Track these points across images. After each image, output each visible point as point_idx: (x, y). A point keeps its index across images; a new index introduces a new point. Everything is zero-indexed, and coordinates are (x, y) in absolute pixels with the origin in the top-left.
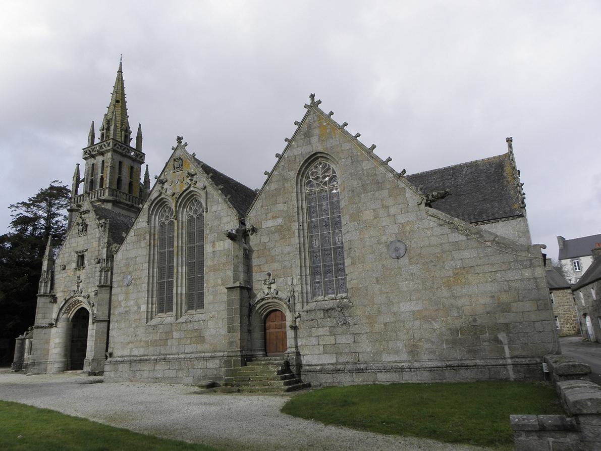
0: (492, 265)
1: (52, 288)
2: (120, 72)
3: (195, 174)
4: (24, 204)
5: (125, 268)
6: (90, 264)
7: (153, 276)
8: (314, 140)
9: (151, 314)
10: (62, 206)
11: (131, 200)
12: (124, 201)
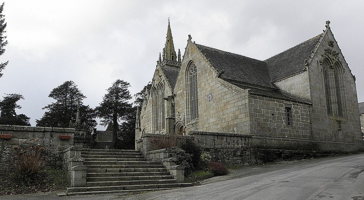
0: (234, 100)
1: (140, 126)
2: (169, 26)
3: (162, 76)
4: (139, 94)
7: (154, 117)
9: (154, 131)
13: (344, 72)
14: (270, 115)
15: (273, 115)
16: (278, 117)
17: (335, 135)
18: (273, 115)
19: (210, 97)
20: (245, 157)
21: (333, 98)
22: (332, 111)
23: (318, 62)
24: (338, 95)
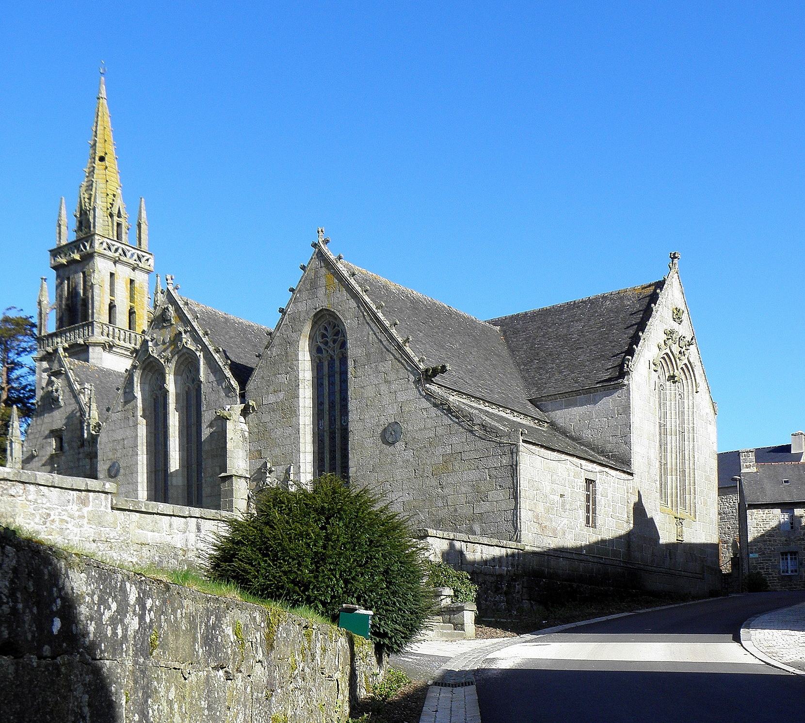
5: (111, 453)
6: (72, 448)
8: (321, 292)
10: (25, 350)
11: (133, 341)
12: (122, 343)
14: (557, 498)
15: (562, 496)
18: (562, 496)
19: (390, 435)
21: (671, 460)
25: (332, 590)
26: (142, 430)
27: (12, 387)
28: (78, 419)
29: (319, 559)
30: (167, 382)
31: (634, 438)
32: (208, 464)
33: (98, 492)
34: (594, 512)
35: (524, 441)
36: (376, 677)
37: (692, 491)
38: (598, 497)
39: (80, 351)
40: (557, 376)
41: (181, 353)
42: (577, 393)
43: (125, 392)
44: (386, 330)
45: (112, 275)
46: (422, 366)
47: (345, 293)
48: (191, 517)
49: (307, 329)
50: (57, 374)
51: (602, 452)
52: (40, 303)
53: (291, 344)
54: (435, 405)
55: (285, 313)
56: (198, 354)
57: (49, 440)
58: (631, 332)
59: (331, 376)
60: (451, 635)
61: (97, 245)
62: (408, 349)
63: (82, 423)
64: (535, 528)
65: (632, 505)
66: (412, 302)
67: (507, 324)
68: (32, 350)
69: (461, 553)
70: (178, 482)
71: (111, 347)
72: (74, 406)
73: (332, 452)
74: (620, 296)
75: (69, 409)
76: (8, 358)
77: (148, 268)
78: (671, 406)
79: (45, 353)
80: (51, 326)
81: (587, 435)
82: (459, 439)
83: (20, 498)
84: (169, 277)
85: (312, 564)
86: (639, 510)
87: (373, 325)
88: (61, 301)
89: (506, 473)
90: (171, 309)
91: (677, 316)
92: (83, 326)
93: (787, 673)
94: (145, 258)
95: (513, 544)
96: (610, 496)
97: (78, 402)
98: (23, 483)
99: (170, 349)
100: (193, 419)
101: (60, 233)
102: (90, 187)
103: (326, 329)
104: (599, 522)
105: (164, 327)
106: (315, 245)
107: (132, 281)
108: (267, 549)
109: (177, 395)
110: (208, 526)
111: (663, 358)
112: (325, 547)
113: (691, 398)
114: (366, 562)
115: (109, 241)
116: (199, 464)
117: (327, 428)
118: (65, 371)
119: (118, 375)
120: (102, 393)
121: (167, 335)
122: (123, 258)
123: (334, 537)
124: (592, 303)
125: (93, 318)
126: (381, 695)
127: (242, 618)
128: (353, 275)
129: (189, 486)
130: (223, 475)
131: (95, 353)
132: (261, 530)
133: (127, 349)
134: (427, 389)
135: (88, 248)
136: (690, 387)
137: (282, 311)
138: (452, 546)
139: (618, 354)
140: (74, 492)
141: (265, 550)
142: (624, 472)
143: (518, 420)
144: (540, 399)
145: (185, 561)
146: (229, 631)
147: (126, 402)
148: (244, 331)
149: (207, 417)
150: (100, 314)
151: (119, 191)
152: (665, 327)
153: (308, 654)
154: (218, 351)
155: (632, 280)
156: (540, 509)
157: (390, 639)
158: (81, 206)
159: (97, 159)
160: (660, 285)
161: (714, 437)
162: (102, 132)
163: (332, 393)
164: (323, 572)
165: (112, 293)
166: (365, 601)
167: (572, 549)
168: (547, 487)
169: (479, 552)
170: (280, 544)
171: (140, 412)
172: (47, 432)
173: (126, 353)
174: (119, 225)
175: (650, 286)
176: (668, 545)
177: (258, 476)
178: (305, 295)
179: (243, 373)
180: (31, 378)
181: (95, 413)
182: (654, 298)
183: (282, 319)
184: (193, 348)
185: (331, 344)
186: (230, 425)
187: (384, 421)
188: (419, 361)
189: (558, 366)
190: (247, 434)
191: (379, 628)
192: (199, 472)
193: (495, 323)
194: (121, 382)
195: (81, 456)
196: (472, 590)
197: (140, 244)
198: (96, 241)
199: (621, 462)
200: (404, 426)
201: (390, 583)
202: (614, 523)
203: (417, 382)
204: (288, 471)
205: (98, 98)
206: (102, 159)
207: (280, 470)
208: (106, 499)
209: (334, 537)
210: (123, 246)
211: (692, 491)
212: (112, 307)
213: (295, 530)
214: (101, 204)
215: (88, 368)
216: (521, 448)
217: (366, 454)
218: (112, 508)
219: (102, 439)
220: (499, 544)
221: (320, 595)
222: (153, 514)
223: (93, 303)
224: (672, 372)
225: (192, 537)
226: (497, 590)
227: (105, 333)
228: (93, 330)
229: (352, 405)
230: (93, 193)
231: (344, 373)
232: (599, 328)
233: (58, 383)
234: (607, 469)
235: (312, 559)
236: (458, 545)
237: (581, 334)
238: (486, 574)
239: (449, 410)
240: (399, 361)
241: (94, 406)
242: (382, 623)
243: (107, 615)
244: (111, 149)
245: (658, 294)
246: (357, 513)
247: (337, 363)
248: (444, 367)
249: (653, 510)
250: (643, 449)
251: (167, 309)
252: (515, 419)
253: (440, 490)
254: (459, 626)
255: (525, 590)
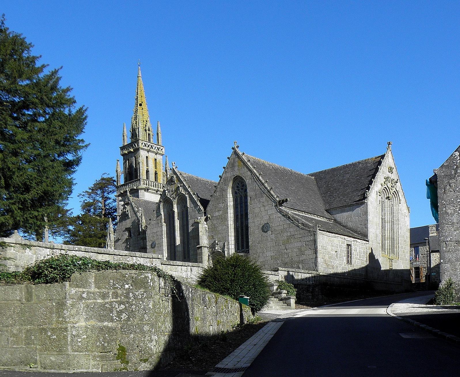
6: (134, 235)
8: (236, 168)
10: (111, 191)
11: (157, 187)
13: (400, 203)
14: (334, 252)
15: (336, 252)
16: (340, 255)
17: (386, 275)
18: (336, 252)
19: (265, 228)
20: (315, 294)
21: (387, 234)
22: (385, 248)
23: (378, 192)
24: (392, 229)
25: (236, 291)
26: (164, 228)
27: (106, 208)
28: (137, 224)
29: (232, 281)
30: (174, 208)
31: (369, 225)
32: (192, 242)
33: (156, 258)
34: (351, 258)
35: (319, 230)
36: (249, 317)
37: (397, 247)
38: (353, 251)
39: (135, 192)
40: (337, 199)
41: (179, 196)
42: (346, 206)
43: (157, 212)
44: (263, 184)
45: (147, 157)
46: (278, 199)
47: (246, 169)
48: (189, 266)
49: (231, 184)
50: (127, 204)
51: (356, 232)
52: (117, 171)
53: (225, 191)
54: (283, 216)
55: (222, 178)
56: (186, 195)
57: (125, 232)
58: (370, 178)
59: (241, 203)
60: (285, 308)
61: (140, 144)
62: (272, 192)
63: (139, 225)
64: (325, 266)
65: (368, 254)
66: (275, 170)
67: (317, 176)
68: (113, 191)
69: (292, 276)
70: (180, 249)
71: (148, 190)
72: (135, 218)
73: (242, 236)
74: (366, 162)
75: (133, 219)
76: (104, 195)
77: (162, 153)
78: (387, 210)
79: (120, 193)
80: (122, 182)
81: (350, 224)
82: (293, 230)
83: (131, 262)
84: (173, 163)
85: (230, 283)
86: (371, 256)
87: (257, 182)
88: (126, 170)
89: (312, 243)
90: (175, 176)
91: (391, 170)
92: (136, 181)
93: (390, 316)
94: (161, 149)
95: (315, 272)
96: (358, 251)
97: (137, 216)
98: (131, 256)
99: (175, 194)
100: (185, 223)
101: (124, 140)
102: (136, 118)
103: (238, 184)
104: (353, 261)
105: (172, 184)
106: (233, 148)
107: (155, 159)
108: (216, 278)
109: (178, 213)
110: (195, 269)
111: (384, 189)
112: (234, 277)
113: (397, 206)
114: (247, 282)
115: (145, 142)
116: (188, 242)
117: (240, 226)
118: (131, 202)
119: (153, 203)
120: (146, 212)
121: (174, 188)
122: (151, 150)
123: (237, 274)
124: (354, 165)
125: (140, 177)
126: (251, 322)
127: (210, 296)
128: (249, 161)
129: (184, 251)
130: (198, 246)
131: (141, 193)
132: (214, 272)
133: (155, 190)
134: (280, 209)
135: (136, 146)
136: (397, 201)
137: (220, 177)
138: (288, 273)
139: (363, 189)
140: (148, 259)
141: (215, 278)
142: (364, 240)
143: (320, 219)
144: (330, 210)
145: (187, 282)
146: (207, 298)
147: (157, 217)
148: (205, 184)
149: (191, 222)
150: (143, 175)
151: (148, 119)
152: (385, 176)
153: (227, 307)
154: (194, 194)
155: (371, 155)
156: (327, 257)
157: (256, 306)
158: (133, 127)
159: (138, 105)
160: (383, 157)
161: (408, 223)
162: (140, 92)
163: (241, 211)
164: (234, 285)
165: (147, 165)
166: (247, 294)
167: (341, 273)
168: (329, 248)
169: (300, 275)
170: (220, 277)
171: (163, 221)
172: (124, 229)
173: (154, 192)
174: (149, 134)
175: (379, 157)
176: (385, 271)
177: (212, 246)
178: (229, 170)
179: (205, 203)
180: (114, 204)
181: (144, 221)
182: (380, 163)
183: (220, 180)
184: (184, 193)
185: (241, 190)
186: (200, 225)
187: (263, 222)
188: (277, 197)
189: (338, 194)
190: (207, 229)
191: (252, 303)
192: (188, 245)
193: (312, 175)
194: (155, 207)
195: (139, 239)
196: (294, 291)
197: (158, 142)
198: (140, 143)
199: (364, 236)
200: (271, 224)
201: (255, 288)
202: (360, 262)
203: (276, 206)
204: (224, 244)
205: (138, 77)
206: (141, 105)
207: (221, 244)
208: (159, 261)
209: (237, 274)
210: (151, 144)
211: (397, 247)
212: (147, 172)
213: (224, 272)
214: (141, 126)
215: (140, 201)
216: (318, 233)
217: (256, 236)
218: (161, 264)
219: (148, 232)
220: (308, 272)
221: (233, 292)
222: (175, 265)
223: (139, 170)
224: (388, 195)
225: (189, 273)
226: (308, 291)
227: (145, 184)
228: (140, 182)
229: (250, 216)
230: (137, 121)
231: (246, 202)
232: (356, 177)
233: (128, 208)
234: (357, 240)
235: (230, 281)
236: (291, 273)
237: (348, 179)
238: (303, 285)
239: (289, 217)
240: (268, 197)
241: (143, 217)
242: (253, 301)
243: (187, 293)
244: (144, 100)
245: (381, 161)
246: (245, 265)
247: (243, 198)
248: (287, 199)
249: (379, 256)
250: (374, 230)
251: (173, 176)
252: (318, 219)
253: (286, 251)
254: (289, 305)
255: (320, 291)
